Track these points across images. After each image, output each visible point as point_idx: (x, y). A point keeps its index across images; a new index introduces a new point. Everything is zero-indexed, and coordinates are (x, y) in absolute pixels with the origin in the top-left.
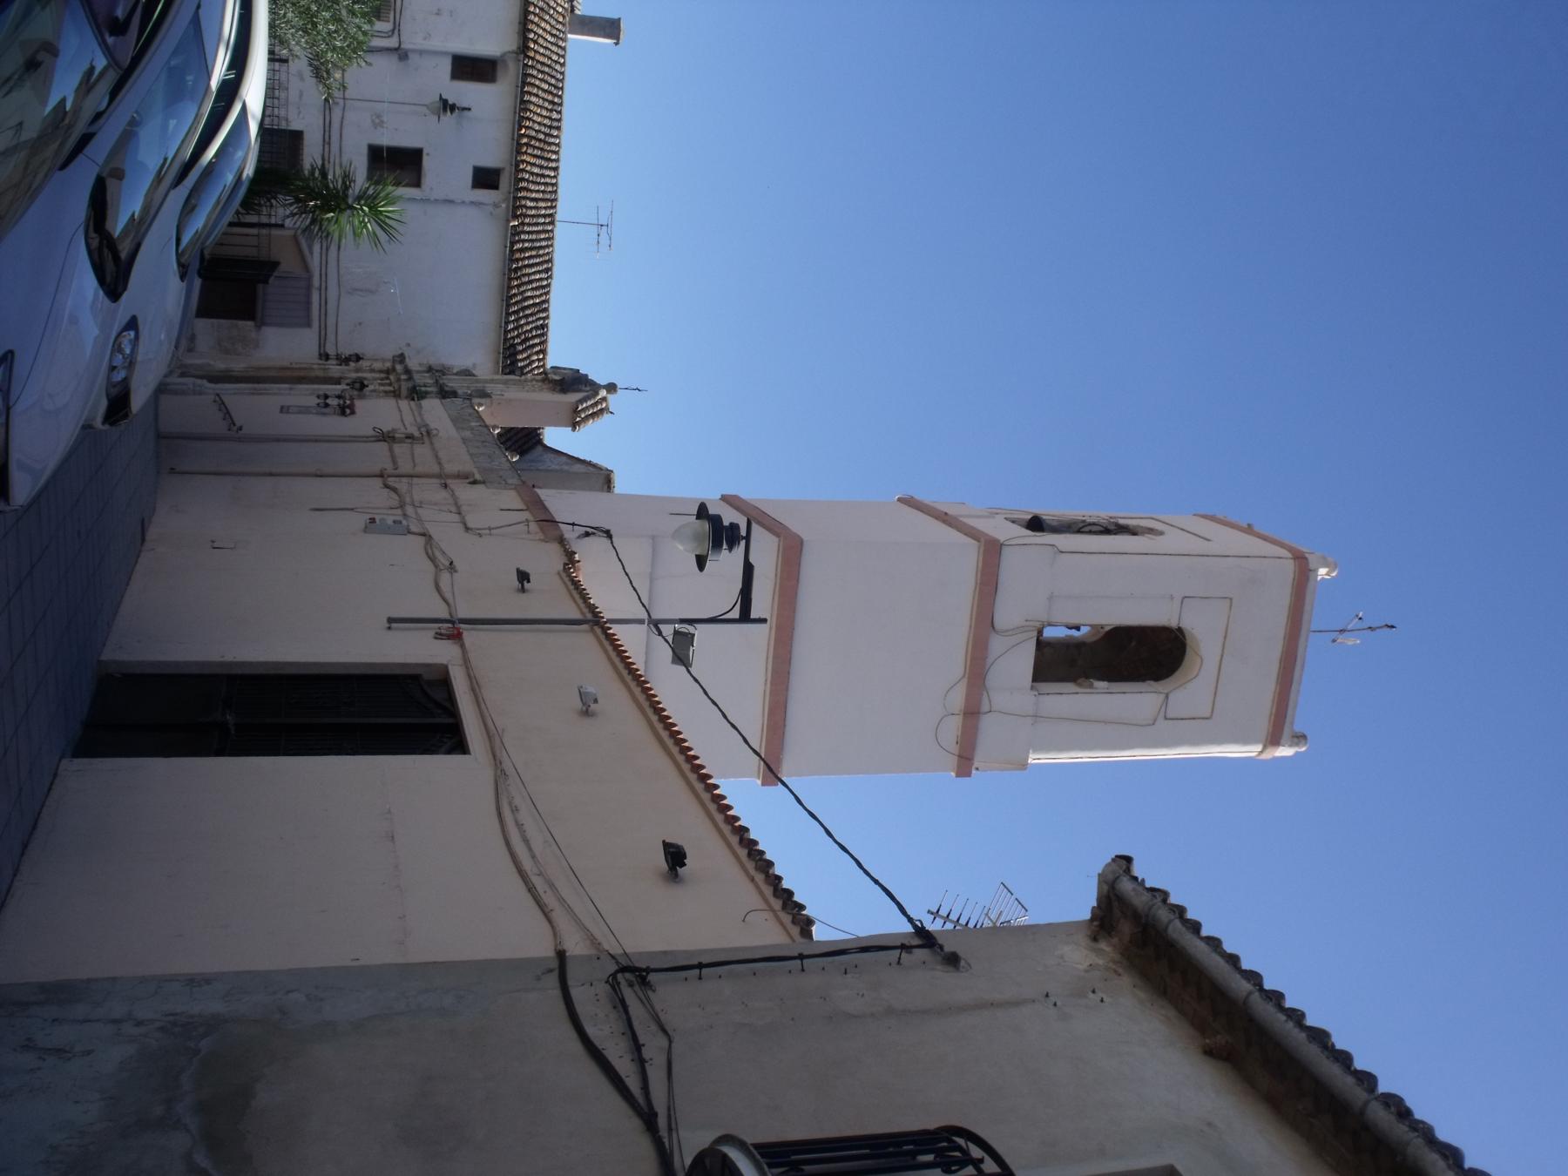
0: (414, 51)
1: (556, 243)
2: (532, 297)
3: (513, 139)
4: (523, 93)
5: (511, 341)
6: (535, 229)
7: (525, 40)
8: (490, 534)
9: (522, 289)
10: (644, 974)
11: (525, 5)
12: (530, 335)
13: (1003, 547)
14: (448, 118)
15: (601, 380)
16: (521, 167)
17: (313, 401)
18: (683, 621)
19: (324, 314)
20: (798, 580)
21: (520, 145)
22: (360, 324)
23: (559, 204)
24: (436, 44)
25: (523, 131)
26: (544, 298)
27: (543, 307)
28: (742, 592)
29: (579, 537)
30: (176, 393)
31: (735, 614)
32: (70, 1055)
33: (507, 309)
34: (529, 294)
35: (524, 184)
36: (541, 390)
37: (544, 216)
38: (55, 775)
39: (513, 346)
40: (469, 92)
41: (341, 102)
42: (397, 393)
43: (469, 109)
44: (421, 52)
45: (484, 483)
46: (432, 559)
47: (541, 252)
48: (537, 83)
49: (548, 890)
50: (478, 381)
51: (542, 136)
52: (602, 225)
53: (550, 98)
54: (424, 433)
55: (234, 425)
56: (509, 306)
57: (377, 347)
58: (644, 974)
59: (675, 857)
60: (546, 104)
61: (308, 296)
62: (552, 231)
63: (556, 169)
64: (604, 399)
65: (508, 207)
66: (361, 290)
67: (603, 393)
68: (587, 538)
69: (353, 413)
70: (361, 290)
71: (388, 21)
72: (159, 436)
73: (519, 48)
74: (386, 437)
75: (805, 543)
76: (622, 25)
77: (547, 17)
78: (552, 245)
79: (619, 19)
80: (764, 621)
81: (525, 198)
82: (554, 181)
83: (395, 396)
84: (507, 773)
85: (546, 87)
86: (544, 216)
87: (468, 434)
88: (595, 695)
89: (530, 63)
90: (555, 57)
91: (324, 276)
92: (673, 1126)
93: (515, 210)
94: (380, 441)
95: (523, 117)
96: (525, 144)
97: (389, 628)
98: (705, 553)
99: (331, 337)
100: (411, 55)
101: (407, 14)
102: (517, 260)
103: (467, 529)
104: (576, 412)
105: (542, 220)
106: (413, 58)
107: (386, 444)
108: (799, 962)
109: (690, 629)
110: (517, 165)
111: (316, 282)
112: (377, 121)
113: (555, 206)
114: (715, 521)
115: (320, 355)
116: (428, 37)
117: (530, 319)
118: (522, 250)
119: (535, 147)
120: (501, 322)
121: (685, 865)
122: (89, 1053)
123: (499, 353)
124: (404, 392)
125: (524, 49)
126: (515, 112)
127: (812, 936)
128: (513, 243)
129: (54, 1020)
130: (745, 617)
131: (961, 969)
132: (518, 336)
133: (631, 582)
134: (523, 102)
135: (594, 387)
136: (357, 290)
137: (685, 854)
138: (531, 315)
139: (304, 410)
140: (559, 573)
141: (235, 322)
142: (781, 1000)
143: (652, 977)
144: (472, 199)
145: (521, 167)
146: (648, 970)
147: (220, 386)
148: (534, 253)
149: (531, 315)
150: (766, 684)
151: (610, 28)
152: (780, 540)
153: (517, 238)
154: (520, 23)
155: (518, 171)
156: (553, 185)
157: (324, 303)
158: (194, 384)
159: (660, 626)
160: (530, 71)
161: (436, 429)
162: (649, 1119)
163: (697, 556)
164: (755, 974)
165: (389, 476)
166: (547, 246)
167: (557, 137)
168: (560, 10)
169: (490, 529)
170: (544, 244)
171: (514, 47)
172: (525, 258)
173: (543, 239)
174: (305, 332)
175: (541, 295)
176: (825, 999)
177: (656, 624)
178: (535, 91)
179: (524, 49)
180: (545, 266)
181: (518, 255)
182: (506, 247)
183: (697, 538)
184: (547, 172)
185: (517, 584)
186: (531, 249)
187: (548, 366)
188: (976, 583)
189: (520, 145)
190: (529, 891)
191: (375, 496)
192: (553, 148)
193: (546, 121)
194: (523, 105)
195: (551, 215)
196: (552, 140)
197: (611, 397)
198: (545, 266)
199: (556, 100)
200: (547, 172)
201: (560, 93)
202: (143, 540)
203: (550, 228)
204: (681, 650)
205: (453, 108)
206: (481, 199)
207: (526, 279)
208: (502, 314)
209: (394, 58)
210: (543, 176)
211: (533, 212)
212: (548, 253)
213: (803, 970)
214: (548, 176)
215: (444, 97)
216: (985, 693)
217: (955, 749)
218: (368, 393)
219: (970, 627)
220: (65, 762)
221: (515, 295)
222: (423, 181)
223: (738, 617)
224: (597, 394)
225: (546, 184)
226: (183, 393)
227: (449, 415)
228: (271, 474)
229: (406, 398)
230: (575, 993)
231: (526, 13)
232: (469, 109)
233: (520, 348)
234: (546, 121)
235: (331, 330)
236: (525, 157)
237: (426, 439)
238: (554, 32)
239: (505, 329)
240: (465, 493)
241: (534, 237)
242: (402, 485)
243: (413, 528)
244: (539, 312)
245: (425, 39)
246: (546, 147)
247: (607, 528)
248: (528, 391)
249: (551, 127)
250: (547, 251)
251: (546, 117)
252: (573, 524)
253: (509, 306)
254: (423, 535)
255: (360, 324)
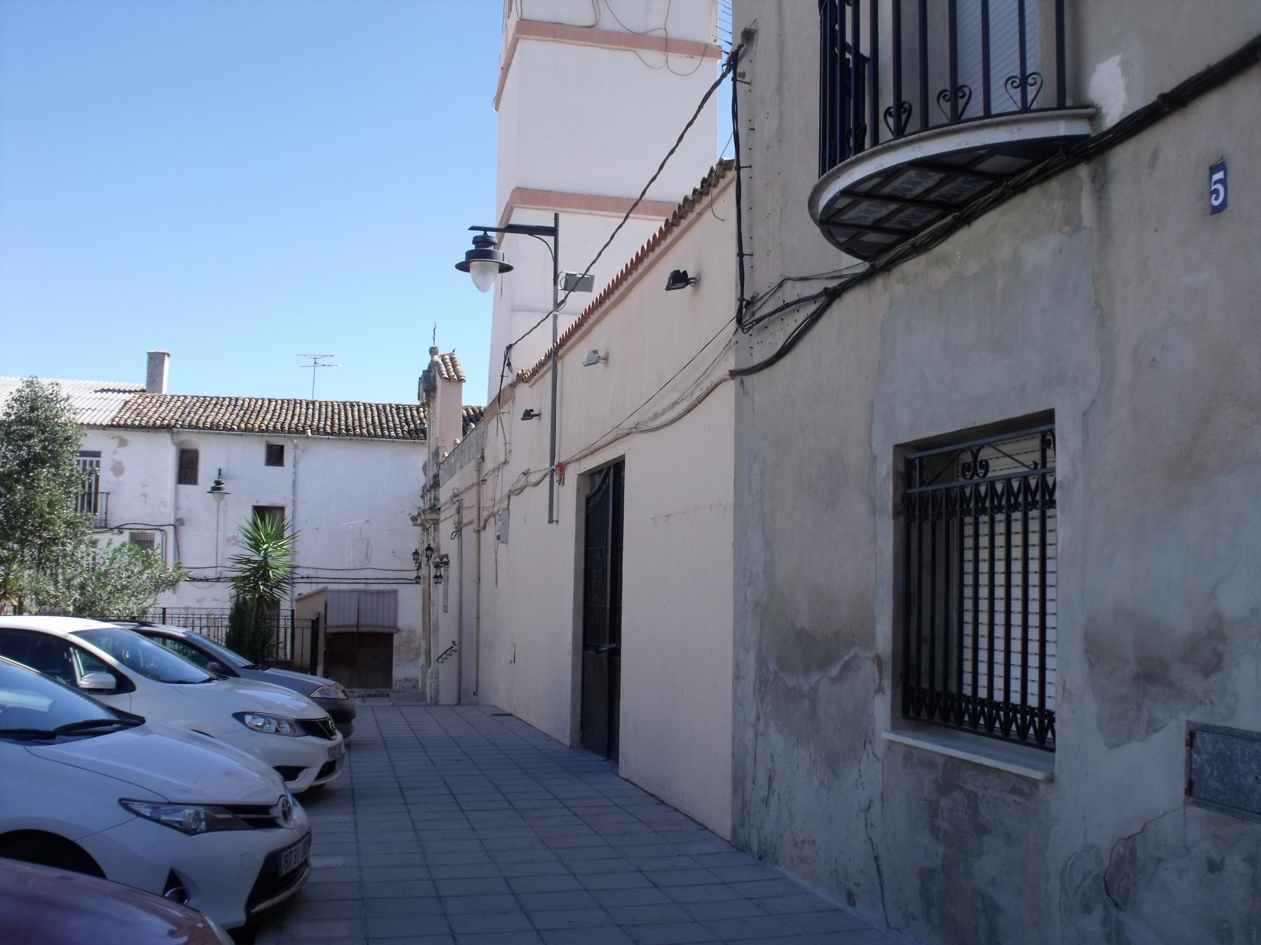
0: (176, 513)
1: (329, 399)
2: (373, 417)
3: (242, 435)
4: (204, 428)
5: (405, 433)
6: (317, 416)
7: (162, 427)
8: (510, 443)
9: (364, 425)
10: (744, 303)
11: (134, 428)
12: (404, 418)
13: (523, 18)
14: (226, 487)
15: (428, 359)
16: (264, 428)
17: (441, 587)
18: (555, 283)
19: (386, 580)
20: (550, 191)
21: (246, 430)
22: (394, 552)
23: (299, 398)
24: (169, 497)
25: (236, 427)
26: (374, 408)
27: (382, 409)
28: (531, 234)
29: (511, 371)
30: (437, 693)
31: (550, 239)
32: (773, 771)
33: (379, 437)
34: (370, 420)
35: (279, 426)
36: (434, 407)
37: (307, 409)
38: (627, 780)
39: (409, 431)
40: (206, 471)
41: (219, 569)
42: (435, 522)
43: (220, 470)
44: (177, 508)
45: (483, 450)
46: (521, 490)
47: (336, 411)
48: (197, 417)
49: (699, 388)
50: (429, 459)
51: (242, 413)
52: (315, 363)
53: (211, 406)
54: (457, 499)
55: (452, 647)
56: (376, 436)
57: (413, 538)
58: (744, 303)
59: (679, 279)
60: (216, 410)
61: (372, 592)
62: (320, 403)
63: (270, 401)
64: (443, 358)
65: (296, 438)
66: (367, 551)
67: (437, 358)
68: (512, 365)
69: (446, 556)
70: (367, 551)
71: (154, 534)
72: (459, 704)
73: (168, 432)
74: (459, 531)
75: (519, 186)
76: (153, 351)
77: (145, 411)
78: (332, 402)
79: (148, 353)
80: (556, 216)
81: (290, 425)
82: (280, 402)
83: (438, 524)
84: (637, 423)
85: (202, 410)
86: (307, 409)
87: (458, 465)
88: (590, 352)
89: (180, 423)
90: (179, 403)
91: (356, 581)
92: (838, 274)
93: (299, 432)
94: (461, 534)
95: (224, 427)
96: (245, 425)
97: (557, 522)
98: (498, 265)
99: (405, 575)
100: (179, 517)
101: (147, 520)
102: (340, 429)
103: (506, 462)
104: (450, 379)
105: (310, 411)
106: (181, 514)
107: (463, 529)
108: (741, 170)
109: (562, 277)
110: (263, 431)
111: (361, 587)
112: (232, 542)
113: (300, 400)
114: (471, 256)
115: (418, 583)
116: (164, 504)
117: (390, 418)
118: (332, 426)
119: (250, 418)
120: (390, 441)
121: (685, 273)
122: (772, 756)
123: (393, 441)
124: (434, 516)
125: (168, 428)
126: (220, 433)
127: (731, 160)
128: (326, 433)
129: (754, 783)
130: (553, 231)
131: (756, 29)
132: (402, 427)
133: (535, 327)
134: (211, 428)
135: (433, 365)
136: (367, 555)
137: (675, 271)
138: (387, 418)
139: (446, 592)
140: (531, 387)
141: (394, 649)
142: (767, 184)
143: (747, 296)
144: (292, 464)
145: (264, 428)
146: (742, 299)
147: (432, 659)
148: (336, 417)
149: (387, 418)
150: (638, 218)
151: (156, 361)
152: (517, 207)
153: (322, 430)
154: (148, 432)
155: (267, 430)
156: (283, 403)
157: (377, 580)
158: (431, 678)
159: (559, 302)
160: (187, 423)
161: (453, 490)
162: (832, 295)
163: (499, 272)
164: (751, 208)
165: (479, 526)
166: (333, 406)
167: (244, 401)
168: (140, 401)
169: (506, 444)
170: (330, 409)
171: (168, 436)
172: (340, 425)
173: (326, 409)
174: (400, 594)
175: (371, 410)
176: (769, 146)
177: (558, 305)
178: (203, 418)
179: (168, 428)
180: (349, 408)
181: (336, 429)
182: (328, 438)
183: (484, 272)
184: (272, 408)
185: (535, 420)
186: (333, 418)
187: (418, 403)
188: (554, 41)
189: (246, 430)
190: (700, 402)
191: (489, 536)
192: (253, 403)
193: (230, 409)
194: (214, 428)
195: (307, 404)
196: (246, 404)
197: (440, 353)
198: (349, 408)
199: (213, 402)
200: (272, 408)
201: (209, 399)
202: (510, 715)
203: (317, 404)
204: (577, 283)
205: (218, 483)
206: (292, 459)
207: (357, 423)
208: (382, 441)
209: (182, 529)
210: (274, 411)
211: (303, 418)
212: (338, 405)
213: (750, 167)
214: (275, 406)
215: (210, 490)
216: (650, 33)
217: (697, 59)
218: (436, 545)
219: (591, 46)
220: (621, 774)
221: (368, 431)
222: (279, 505)
223: (553, 237)
224: (437, 362)
225: (281, 408)
226: (437, 686)
227: (449, 479)
228: (478, 618)
229: (438, 514)
230: (757, 360)
231: (140, 427)
232: (220, 470)
233: (412, 426)
234: (230, 409)
235: (398, 575)
236: (256, 426)
237: (460, 498)
238: (158, 405)
239: (395, 438)
240: (489, 465)
241: (323, 417)
242: (484, 514)
243: (505, 506)
244: (385, 412)
245: (166, 506)
246: (251, 409)
247: (505, 349)
248: (435, 418)
249: (235, 406)
250: (336, 407)
251: (226, 410)
252: (502, 376)
253: (376, 436)
254: (509, 497)
255: (394, 552)
